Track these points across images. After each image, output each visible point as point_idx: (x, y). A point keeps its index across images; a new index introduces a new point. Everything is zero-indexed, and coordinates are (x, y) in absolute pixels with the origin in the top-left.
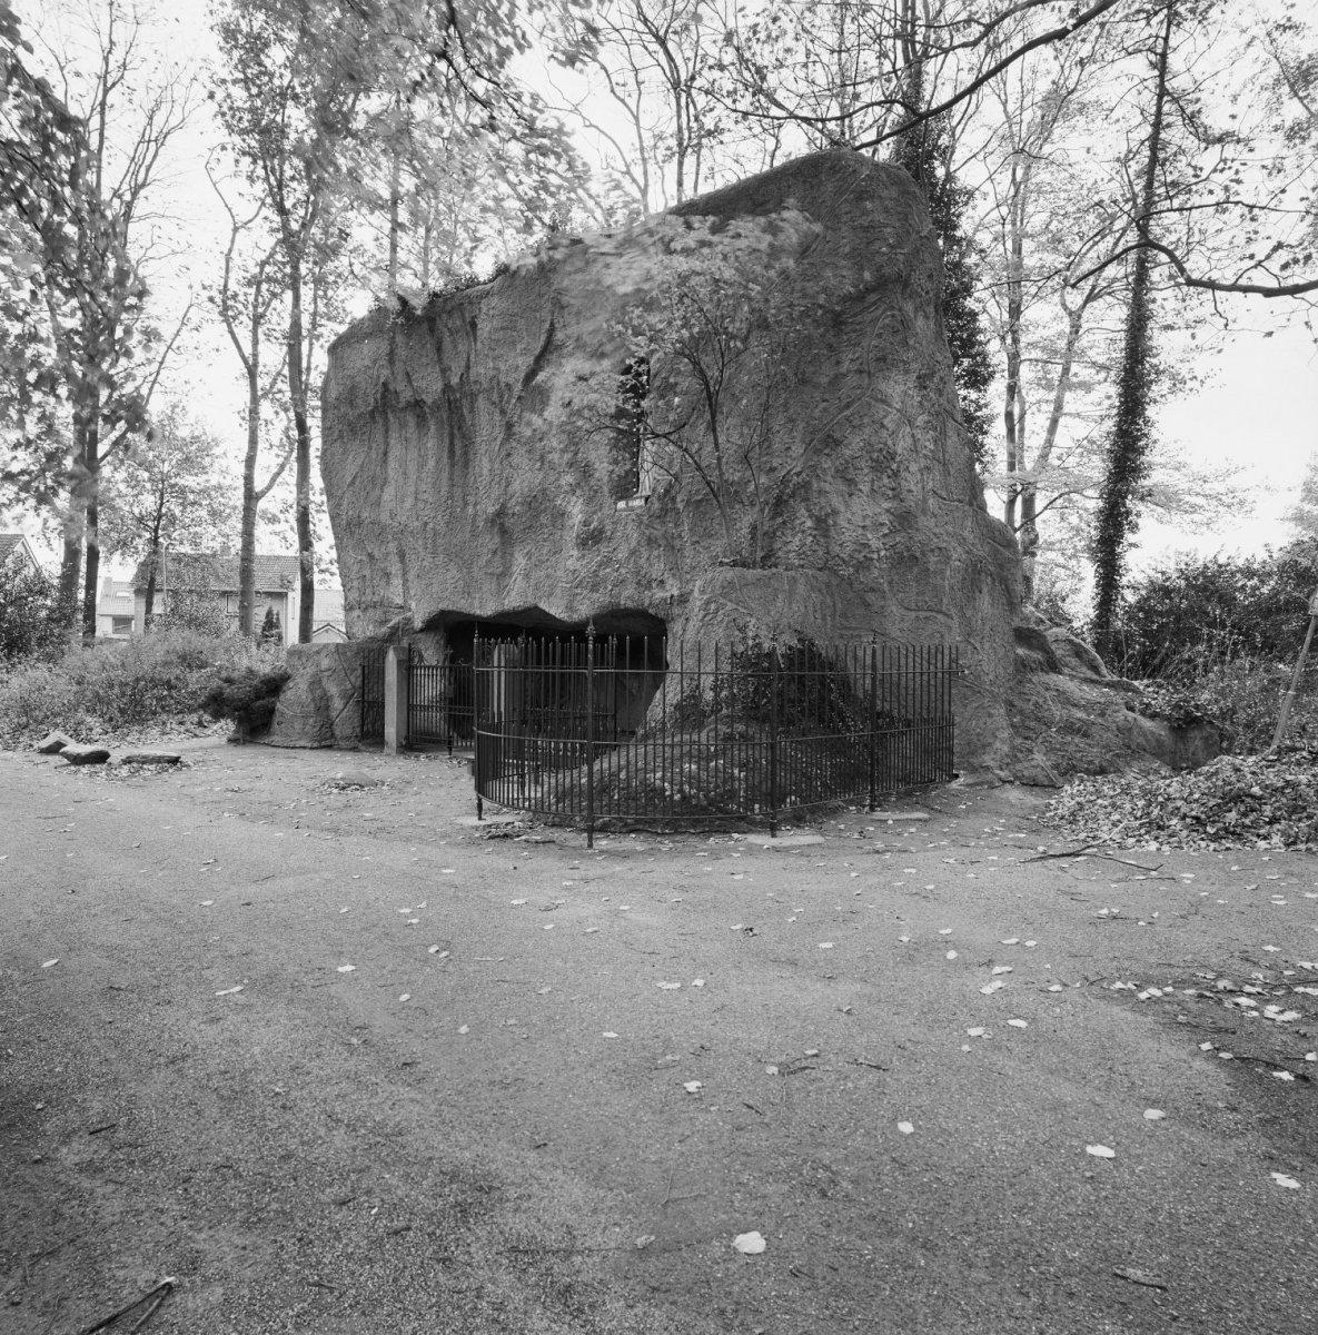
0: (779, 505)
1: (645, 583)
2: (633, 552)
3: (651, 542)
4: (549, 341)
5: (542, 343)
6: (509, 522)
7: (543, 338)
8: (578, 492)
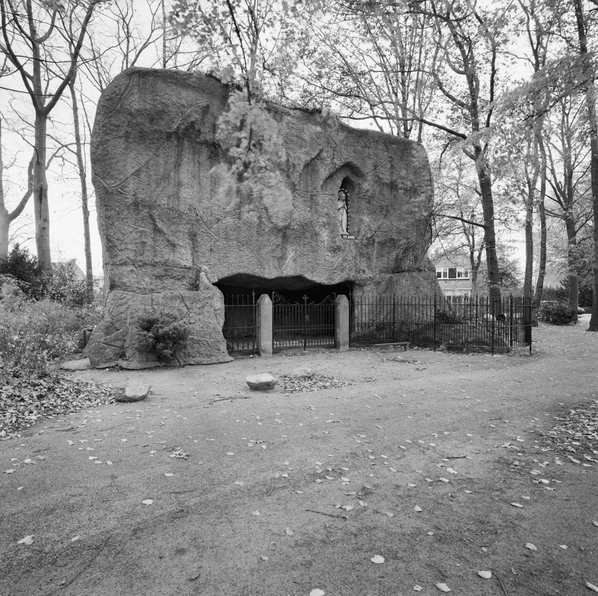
0: (406, 250)
1: (358, 271)
2: (354, 257)
3: (361, 255)
4: (319, 154)
5: (316, 154)
6: (289, 232)
7: (317, 152)
8: (327, 227)
